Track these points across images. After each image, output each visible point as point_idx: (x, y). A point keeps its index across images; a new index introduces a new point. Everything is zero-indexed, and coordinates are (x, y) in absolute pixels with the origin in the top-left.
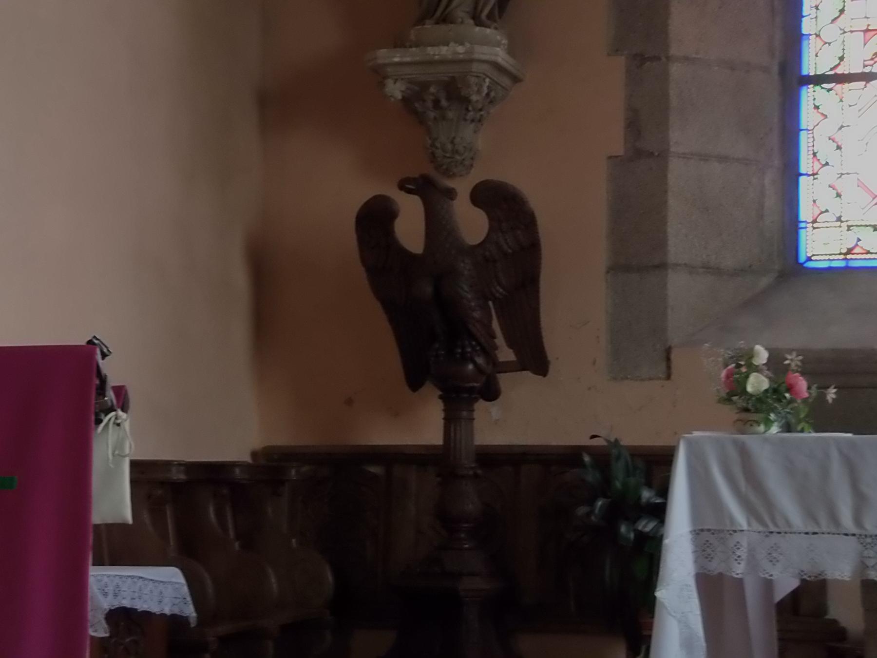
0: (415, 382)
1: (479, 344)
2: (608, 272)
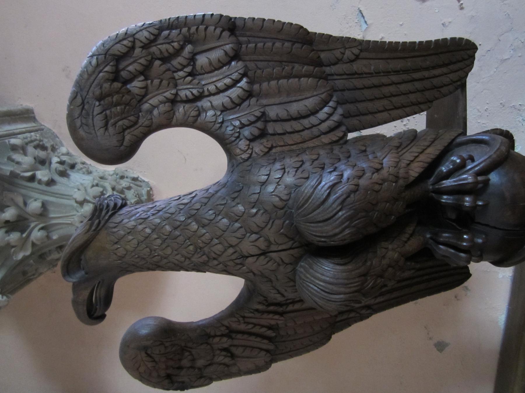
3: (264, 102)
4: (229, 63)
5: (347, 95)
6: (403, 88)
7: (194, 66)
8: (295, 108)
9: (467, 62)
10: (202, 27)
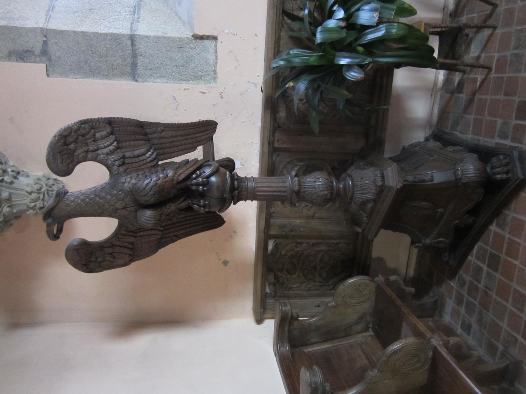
0: (219, 222)
1: (194, 172)
2: (137, 81)
3: (123, 150)
4: (109, 136)
5: (159, 146)
6: (183, 142)
7: (95, 138)
8: (136, 153)
9: (213, 130)
10: (98, 123)
